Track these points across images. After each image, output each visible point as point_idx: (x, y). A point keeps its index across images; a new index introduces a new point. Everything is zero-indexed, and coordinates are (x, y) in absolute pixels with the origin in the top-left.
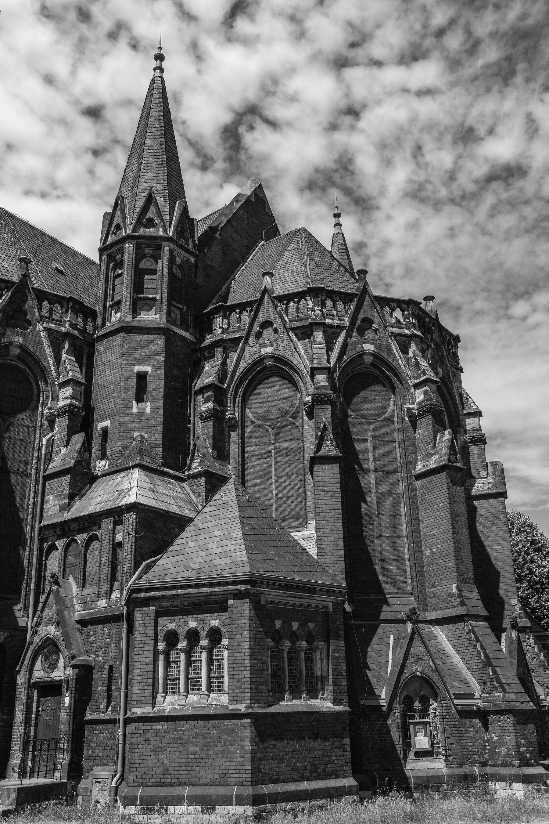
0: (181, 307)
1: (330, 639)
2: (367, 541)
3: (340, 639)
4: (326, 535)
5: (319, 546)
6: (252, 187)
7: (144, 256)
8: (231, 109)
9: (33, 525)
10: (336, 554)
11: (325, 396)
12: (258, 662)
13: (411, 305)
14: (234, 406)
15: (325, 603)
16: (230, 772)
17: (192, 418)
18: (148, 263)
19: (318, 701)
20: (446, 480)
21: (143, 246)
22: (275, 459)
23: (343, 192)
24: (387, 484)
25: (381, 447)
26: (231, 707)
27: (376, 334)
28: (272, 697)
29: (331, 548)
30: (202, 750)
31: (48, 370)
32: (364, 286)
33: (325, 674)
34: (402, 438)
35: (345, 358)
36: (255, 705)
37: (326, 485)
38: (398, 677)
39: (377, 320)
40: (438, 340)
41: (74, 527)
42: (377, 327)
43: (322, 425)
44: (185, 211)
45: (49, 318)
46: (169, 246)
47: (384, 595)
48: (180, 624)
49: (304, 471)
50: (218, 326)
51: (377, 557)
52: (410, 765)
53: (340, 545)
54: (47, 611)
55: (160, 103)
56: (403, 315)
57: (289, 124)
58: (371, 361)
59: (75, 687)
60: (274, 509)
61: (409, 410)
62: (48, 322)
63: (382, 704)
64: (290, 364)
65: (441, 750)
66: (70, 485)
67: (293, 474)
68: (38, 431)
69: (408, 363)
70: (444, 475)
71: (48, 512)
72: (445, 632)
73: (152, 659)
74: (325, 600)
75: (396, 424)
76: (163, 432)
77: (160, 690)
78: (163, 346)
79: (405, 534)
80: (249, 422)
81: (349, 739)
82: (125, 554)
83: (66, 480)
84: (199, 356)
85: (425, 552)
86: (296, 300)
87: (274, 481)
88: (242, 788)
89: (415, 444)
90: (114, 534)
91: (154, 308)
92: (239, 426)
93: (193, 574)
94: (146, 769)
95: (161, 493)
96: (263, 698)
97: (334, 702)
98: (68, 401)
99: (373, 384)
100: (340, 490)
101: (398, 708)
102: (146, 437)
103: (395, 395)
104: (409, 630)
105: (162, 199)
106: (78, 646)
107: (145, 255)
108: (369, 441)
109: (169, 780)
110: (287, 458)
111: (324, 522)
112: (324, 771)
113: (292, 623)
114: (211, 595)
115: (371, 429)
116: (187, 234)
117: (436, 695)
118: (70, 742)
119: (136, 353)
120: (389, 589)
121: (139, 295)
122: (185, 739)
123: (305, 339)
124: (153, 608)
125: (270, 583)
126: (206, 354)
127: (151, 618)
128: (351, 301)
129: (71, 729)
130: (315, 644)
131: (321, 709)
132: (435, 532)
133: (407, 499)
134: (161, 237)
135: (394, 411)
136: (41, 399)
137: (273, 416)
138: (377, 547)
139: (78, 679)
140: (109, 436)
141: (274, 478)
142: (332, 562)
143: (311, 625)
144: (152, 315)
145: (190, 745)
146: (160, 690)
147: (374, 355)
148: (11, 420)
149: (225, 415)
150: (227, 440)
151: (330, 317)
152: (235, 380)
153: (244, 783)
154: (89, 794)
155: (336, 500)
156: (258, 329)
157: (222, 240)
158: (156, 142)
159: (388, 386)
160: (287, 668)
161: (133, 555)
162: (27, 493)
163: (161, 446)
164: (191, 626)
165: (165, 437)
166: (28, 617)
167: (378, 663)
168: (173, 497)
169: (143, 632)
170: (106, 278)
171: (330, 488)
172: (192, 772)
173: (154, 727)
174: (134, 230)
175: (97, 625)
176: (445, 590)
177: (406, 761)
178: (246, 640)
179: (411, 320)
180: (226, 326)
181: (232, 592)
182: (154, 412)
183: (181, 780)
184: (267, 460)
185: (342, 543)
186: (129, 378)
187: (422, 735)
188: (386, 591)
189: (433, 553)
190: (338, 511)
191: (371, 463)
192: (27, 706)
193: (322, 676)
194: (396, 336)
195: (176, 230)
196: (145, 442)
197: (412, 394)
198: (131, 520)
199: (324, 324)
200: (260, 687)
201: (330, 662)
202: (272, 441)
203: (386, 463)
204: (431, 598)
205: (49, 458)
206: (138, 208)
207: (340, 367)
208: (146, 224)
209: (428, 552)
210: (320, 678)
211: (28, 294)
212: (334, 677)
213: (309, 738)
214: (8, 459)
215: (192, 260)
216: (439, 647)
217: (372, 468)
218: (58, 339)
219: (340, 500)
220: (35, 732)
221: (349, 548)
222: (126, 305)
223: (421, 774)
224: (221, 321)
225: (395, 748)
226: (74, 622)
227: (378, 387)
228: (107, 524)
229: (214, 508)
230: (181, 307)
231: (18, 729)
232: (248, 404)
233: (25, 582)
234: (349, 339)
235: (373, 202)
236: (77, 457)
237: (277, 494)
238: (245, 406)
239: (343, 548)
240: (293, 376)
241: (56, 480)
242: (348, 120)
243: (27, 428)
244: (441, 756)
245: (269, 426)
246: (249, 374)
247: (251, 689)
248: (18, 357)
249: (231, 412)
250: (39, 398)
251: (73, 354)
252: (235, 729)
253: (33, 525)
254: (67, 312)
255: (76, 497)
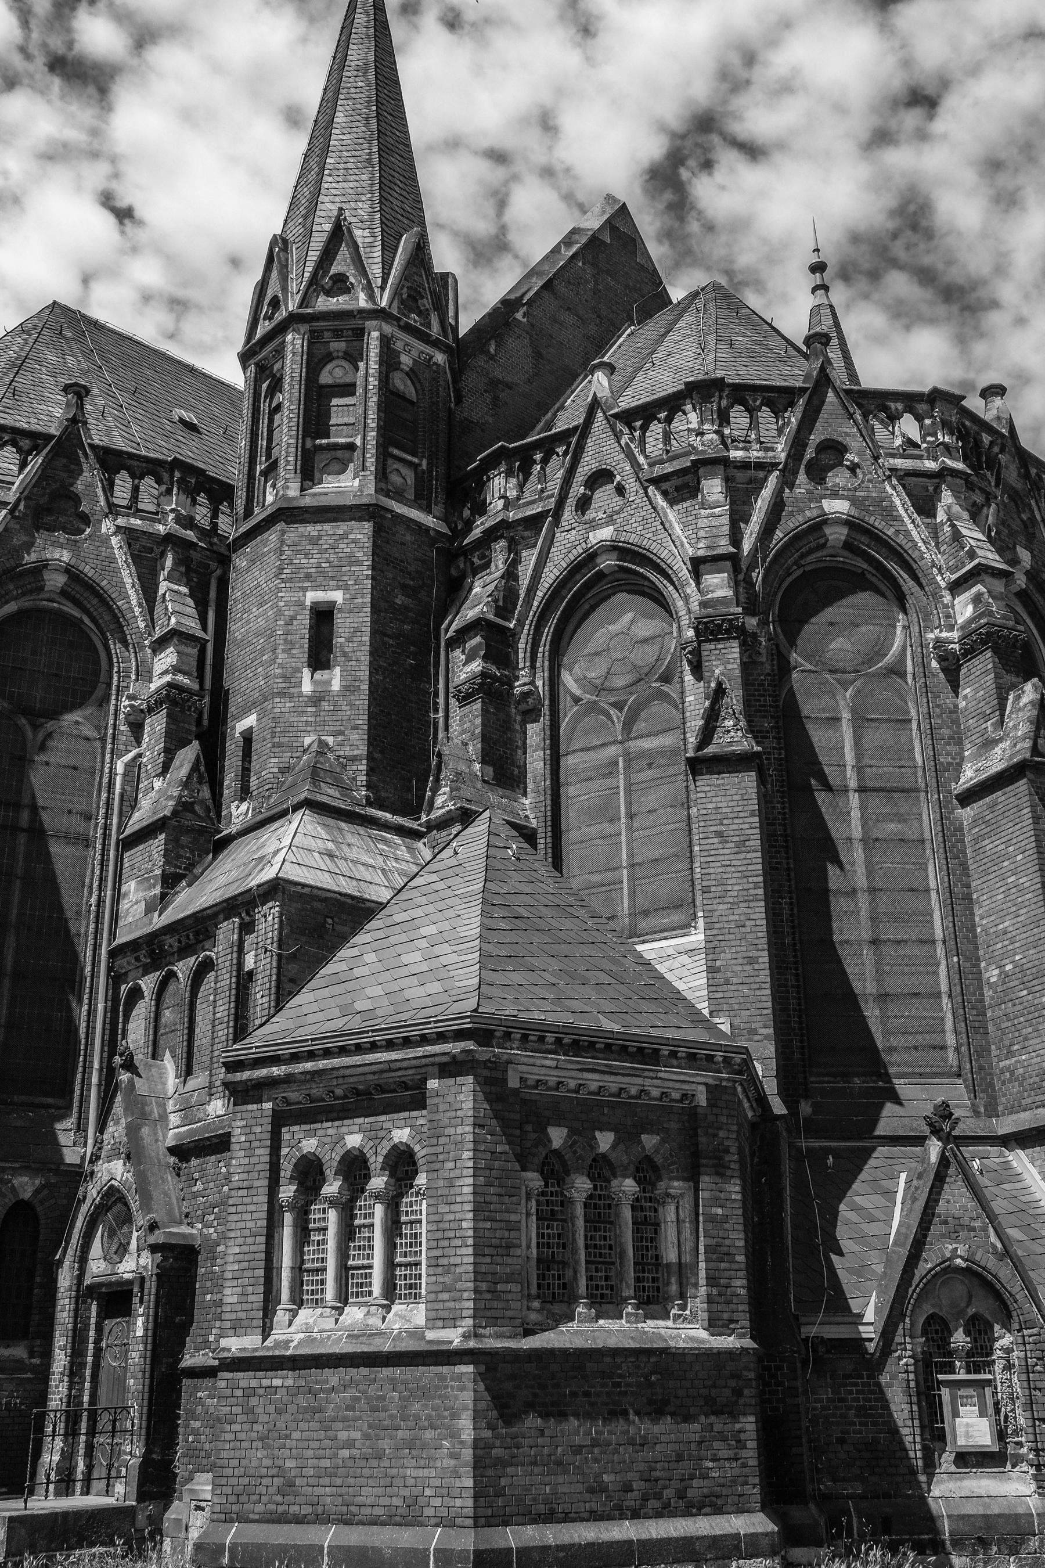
0: (416, 460)
1: (699, 1174)
2: (844, 953)
3: (729, 1173)
4: (727, 937)
5: (710, 963)
6: (604, 212)
7: (329, 358)
8: (662, 128)
9: (96, 947)
10: (752, 980)
11: (723, 621)
12: (496, 1225)
13: (938, 404)
14: (533, 667)
15: (686, 1087)
16: (428, 1492)
17: (441, 700)
18: (338, 373)
19: (670, 1323)
20: (1027, 798)
21: (326, 334)
22: (627, 779)
23: (915, 278)
24: (891, 821)
25: (874, 737)
26: (430, 1335)
27: (855, 476)
28: (538, 1311)
29: (739, 968)
30: (366, 1437)
31: (128, 616)
32: (822, 369)
33: (687, 1258)
34: (925, 710)
35: (779, 534)
36: (487, 1331)
37: (725, 822)
38: (905, 1271)
39: (855, 443)
40: (1019, 486)
41: (171, 946)
42: (856, 460)
43: (713, 685)
44: (420, 255)
45: (130, 508)
46: (380, 330)
47: (887, 1078)
48: (327, 1140)
49: (688, 797)
50: (497, 495)
51: (869, 991)
52: (943, 1487)
53: (760, 960)
54: (111, 1128)
55: (368, 37)
56: (921, 427)
57: (781, 146)
58: (843, 538)
59: (157, 1294)
60: (626, 891)
61: (939, 643)
62: (128, 515)
63: (864, 1336)
64: (651, 560)
65: (1024, 1450)
66: (164, 856)
67: (663, 806)
68: (109, 746)
69: (936, 538)
70: (1022, 786)
71: (125, 917)
72: (1039, 1162)
73: (264, 1223)
74: (688, 1079)
75: (910, 680)
76: (369, 729)
77: (285, 1295)
78: (368, 544)
79: (939, 934)
80: (569, 699)
81: (752, 1419)
82: (259, 996)
83: (157, 844)
84: (462, 566)
85: (987, 975)
86: (662, 415)
87: (623, 826)
88: (452, 1532)
89: (957, 722)
90: (241, 949)
91: (351, 465)
92: (546, 710)
93: (355, 1023)
94: (246, 1480)
95: (352, 861)
96: (509, 1313)
97: (710, 1326)
98: (168, 678)
99: (852, 592)
100: (758, 831)
101: (909, 1347)
102: (331, 744)
103: (906, 613)
104: (934, 1157)
105: (366, 233)
106: (168, 1204)
107: (331, 353)
108: (844, 722)
109: (294, 1509)
110: (650, 774)
111: (721, 907)
112: (681, 1495)
113: (597, 1134)
114: (390, 1070)
115: (848, 694)
116: (426, 303)
117: (1009, 1316)
118: (144, 1417)
119: (308, 563)
120: (898, 1066)
121: (318, 442)
122: (330, 1412)
123: (684, 500)
124: (268, 1106)
125: (531, 1038)
126: (475, 560)
127: (264, 1128)
128: (792, 404)
129: (147, 1388)
130: (662, 1185)
131: (672, 1344)
132: (1006, 924)
133: (942, 850)
134: (361, 311)
135: (904, 650)
136: (115, 678)
137: (620, 682)
138: (867, 967)
139: (163, 1275)
140: (255, 746)
141: (623, 820)
142: (741, 1000)
143: (650, 1141)
144: (347, 480)
145: (340, 1424)
146: (285, 1295)
147: (850, 524)
148: (51, 725)
149: (512, 687)
150: (520, 743)
151: (741, 445)
152: (534, 608)
153: (459, 1521)
154: (183, 1535)
155: (749, 855)
156: (582, 490)
157: (532, 325)
158: (358, 118)
159: (888, 594)
160: (581, 1242)
161: (273, 997)
162: (87, 881)
163: (365, 762)
164: (349, 1146)
165: (372, 742)
166: (85, 1145)
167: (861, 1239)
168: (383, 870)
169: (246, 1161)
170: (253, 414)
171: (735, 827)
172: (344, 1490)
173: (266, 1382)
174: (304, 302)
175: (206, 1155)
176: (1034, 1061)
177: (931, 1476)
178: (465, 1172)
179: (940, 437)
180: (515, 493)
181: (437, 1059)
182: (349, 689)
183: (320, 1509)
184: (608, 782)
185: (766, 953)
186: (293, 618)
187: (973, 1412)
188: (892, 1070)
189: (1005, 976)
190: (755, 879)
191: (849, 772)
192: (74, 1337)
193: (680, 1264)
194: (904, 476)
195: (396, 294)
196: (329, 755)
197: (946, 606)
198: (270, 918)
199: (724, 462)
200: (500, 1287)
201: (701, 1230)
202: (620, 738)
203: (887, 770)
204: (1003, 1083)
205: (130, 803)
206: (313, 256)
207: (767, 556)
208: (331, 288)
209: (993, 975)
210: (675, 1269)
211: (83, 460)
212: (712, 1265)
213: (638, 1413)
214: (44, 808)
215: (440, 358)
216: (1024, 1199)
217: (853, 784)
218: (151, 551)
219: (759, 854)
220: (93, 1395)
221: (796, 969)
222: (288, 462)
223: (970, 1509)
224: (503, 483)
225: (901, 1442)
226: (163, 1151)
227: (864, 598)
228: (227, 931)
229: (434, 877)
230: (416, 460)
231: (57, 1387)
232: (565, 660)
233: (80, 1069)
234: (787, 490)
235: (982, 293)
236: (180, 797)
237: (631, 855)
238: (559, 666)
239: (767, 966)
240: (660, 586)
241: (141, 847)
242: (911, 118)
243: (86, 743)
244: (1024, 1466)
245: (611, 704)
246: (564, 592)
247: (476, 1291)
248: (63, 593)
249: (527, 680)
250: (111, 678)
251: (184, 580)
252: (437, 1388)
253: (96, 947)
254: (169, 492)
255: (180, 881)
